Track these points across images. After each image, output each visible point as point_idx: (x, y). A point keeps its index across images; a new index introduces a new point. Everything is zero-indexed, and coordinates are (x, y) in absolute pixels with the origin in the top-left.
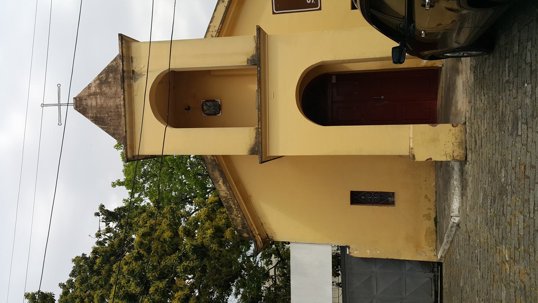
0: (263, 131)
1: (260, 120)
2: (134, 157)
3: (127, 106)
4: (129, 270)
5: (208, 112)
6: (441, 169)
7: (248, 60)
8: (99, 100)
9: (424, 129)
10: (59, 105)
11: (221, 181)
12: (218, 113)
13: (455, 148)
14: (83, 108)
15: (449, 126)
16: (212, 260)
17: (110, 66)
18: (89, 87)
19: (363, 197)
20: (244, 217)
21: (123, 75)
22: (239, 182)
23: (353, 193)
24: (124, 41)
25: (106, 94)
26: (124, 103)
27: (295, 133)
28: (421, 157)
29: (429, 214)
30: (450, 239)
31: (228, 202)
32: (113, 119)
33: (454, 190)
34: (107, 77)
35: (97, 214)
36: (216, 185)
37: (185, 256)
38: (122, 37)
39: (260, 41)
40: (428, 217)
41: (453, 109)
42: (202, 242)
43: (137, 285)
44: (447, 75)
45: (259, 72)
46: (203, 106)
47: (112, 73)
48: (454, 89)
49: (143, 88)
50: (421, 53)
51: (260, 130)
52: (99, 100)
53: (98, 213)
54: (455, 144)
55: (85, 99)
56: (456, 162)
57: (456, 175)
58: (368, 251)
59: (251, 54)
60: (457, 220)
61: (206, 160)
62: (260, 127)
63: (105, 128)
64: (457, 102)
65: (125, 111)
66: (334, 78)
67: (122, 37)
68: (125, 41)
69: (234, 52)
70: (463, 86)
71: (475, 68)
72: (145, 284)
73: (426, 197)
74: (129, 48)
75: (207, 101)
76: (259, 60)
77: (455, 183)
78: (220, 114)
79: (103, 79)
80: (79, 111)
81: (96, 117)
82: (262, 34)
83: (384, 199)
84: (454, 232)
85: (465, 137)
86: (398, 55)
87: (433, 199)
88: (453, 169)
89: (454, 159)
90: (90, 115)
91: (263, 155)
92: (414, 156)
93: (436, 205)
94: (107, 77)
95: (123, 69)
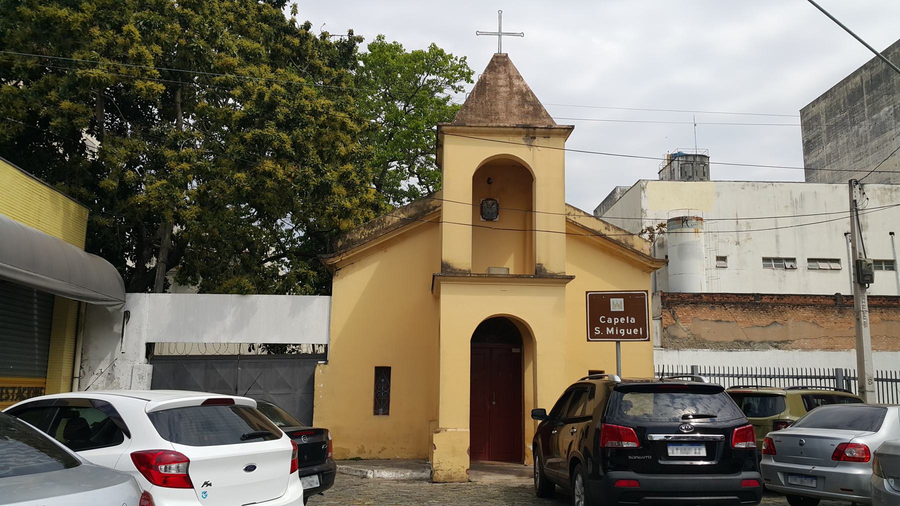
2: (442, 133)
3: (498, 129)
5: (485, 205)
6: (421, 460)
10: (500, 34)
14: (496, 67)
15: (468, 466)
18: (519, 77)
20: (361, 242)
22: (403, 237)
23: (388, 369)
27: (463, 313)
28: (437, 439)
30: (344, 471)
31: (378, 223)
35: (351, 33)
37: (318, 172)
38: (570, 129)
40: (362, 450)
45: (529, 277)
46: (492, 199)
49: (519, 150)
57: (416, 474)
60: (370, 475)
61: (428, 200)
65: (492, 127)
66: (518, 351)
67: (570, 129)
68: (568, 130)
69: (551, 249)
72: (287, 125)
73: (384, 449)
74: (559, 135)
75: (498, 205)
76: (541, 277)
77: (408, 474)
79: (527, 99)
80: (492, 61)
81: (485, 84)
83: (382, 403)
86: (538, 414)
87: (381, 456)
90: (488, 76)
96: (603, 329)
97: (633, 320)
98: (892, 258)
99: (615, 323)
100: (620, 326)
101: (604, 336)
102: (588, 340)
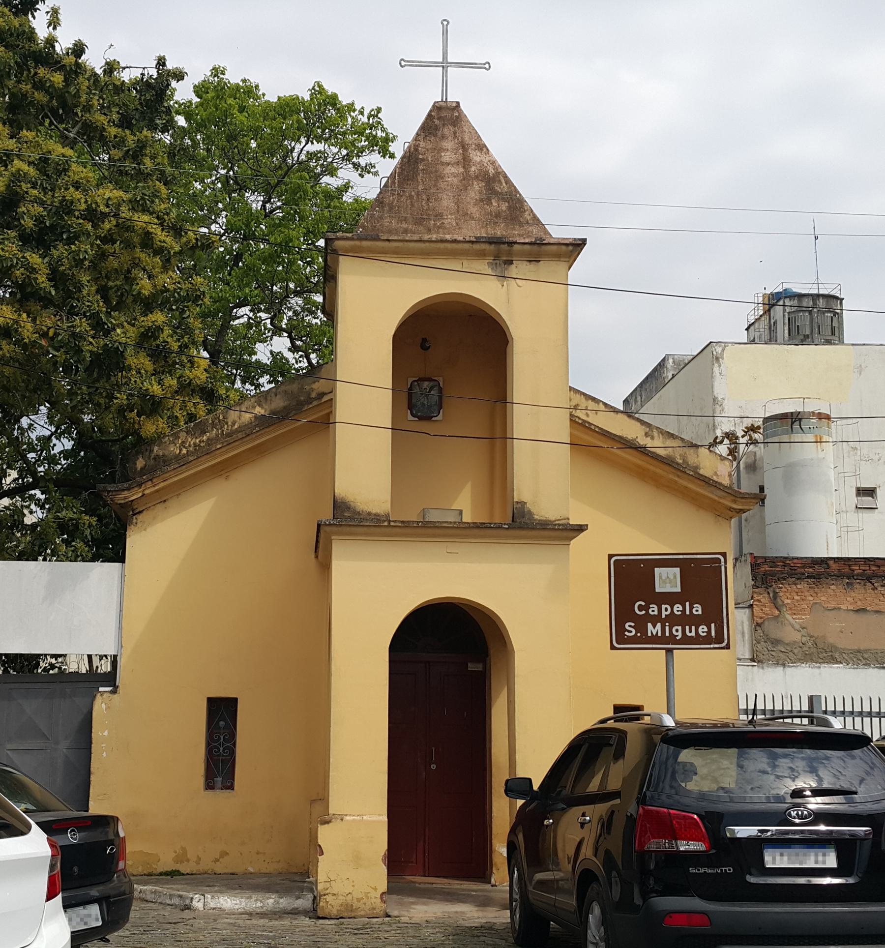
0: (383, 530)
1: (406, 524)
2: (335, 252)
3: (442, 245)
4: (72, 202)
5: (416, 390)
6: (296, 875)
7: (523, 504)
8: (453, 170)
9: (378, 841)
10: (444, 65)
11: (263, 412)
12: (412, 414)
13: (341, 897)
14: (437, 128)
15: (383, 887)
16: (89, 387)
17: (522, 206)
18: (482, 147)
19: (222, 723)
20: (181, 461)
21: (504, 243)
22: (260, 452)
24: (571, 248)
25: (466, 189)
26: (447, 241)
27: (375, 596)
28: (325, 835)
29: (188, 860)
31: (214, 425)
32: (412, 205)
33: (256, 900)
34: (502, 197)
36: (253, 400)
37: (99, 326)
38: (579, 245)
39: (558, 529)
40: (182, 857)
41: (411, 900)
42: (130, 369)
43: (39, 220)
44: (473, 891)
45: (499, 527)
46: (430, 380)
47: (509, 208)
48: (448, 901)
50: (520, 828)
51: (386, 524)
52: (453, 170)
53: (164, 65)
54: (350, 896)
55: (455, 133)
56: (310, 901)
57: (285, 902)
58: (106, 733)
59: (534, 510)
60: (198, 904)
61: (309, 380)
62: (392, 524)
63: (393, 182)
64: (424, 904)
66: (479, 667)
67: (579, 245)
70: (456, 912)
71: (491, 928)
72: (39, 239)
73: (224, 854)
74: (558, 256)
75: (440, 390)
77: (271, 901)
78: (410, 417)
79: (496, 187)
80: (429, 116)
81: (417, 161)
82: (571, 534)
83: (220, 767)
84: (168, 902)
85: (362, 916)
86: (517, 787)
87: (219, 868)
88: (298, 898)
89: (321, 896)
90: (422, 144)
91: (334, 529)
92: (327, 822)
93: (206, 873)
94: (502, 197)
95: (515, 243)
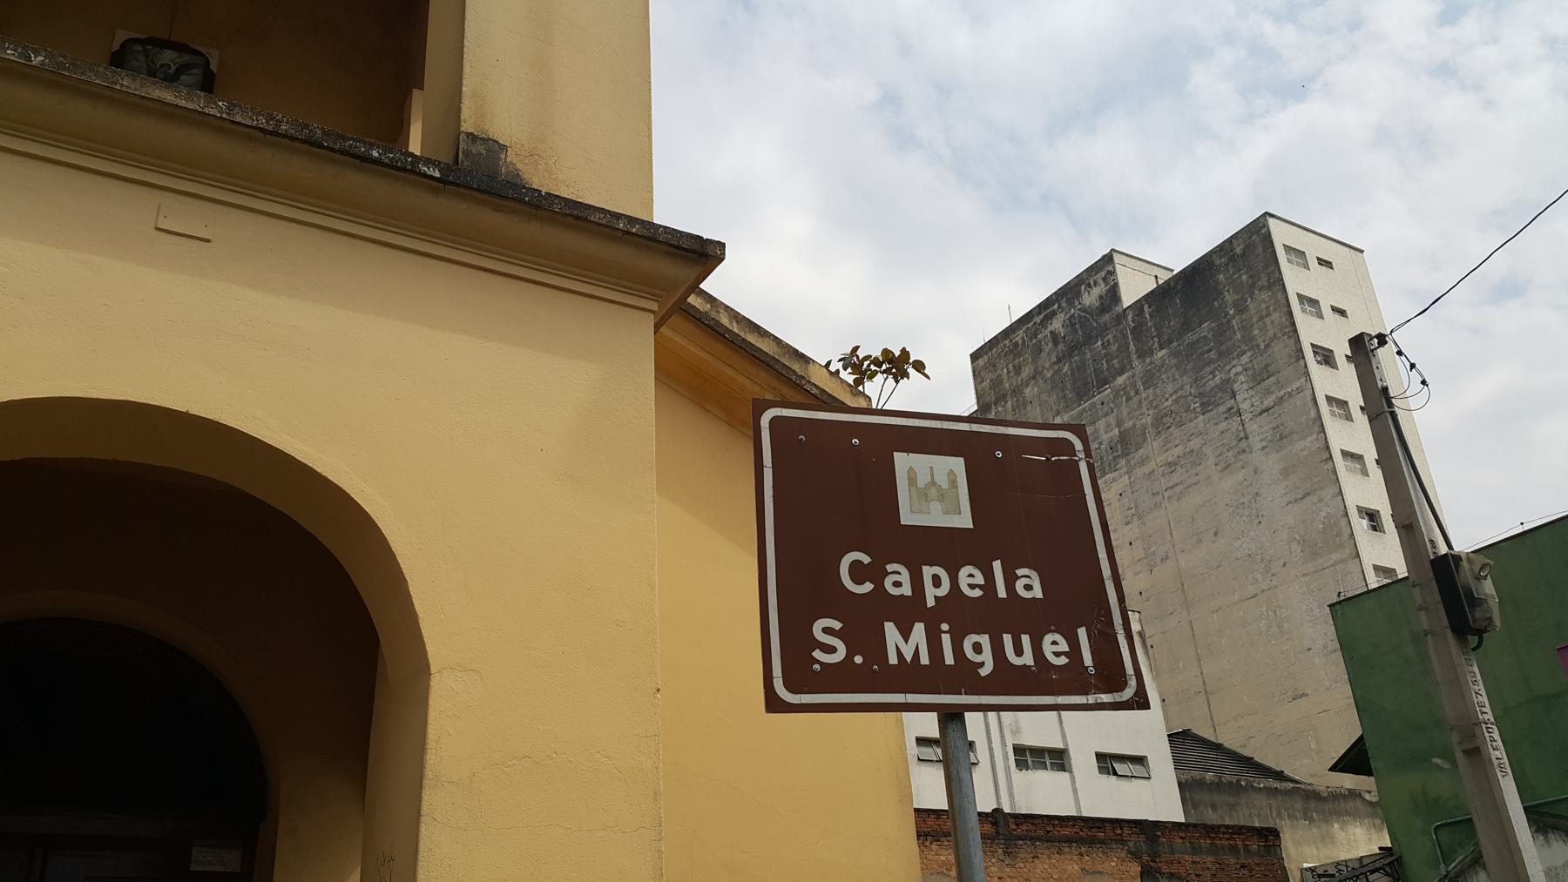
46: (182, 48)
96: (862, 635)
97: (1030, 584)
98: (1058, 744)
99: (931, 594)
100: (958, 614)
101: (872, 679)
102: (774, 704)
